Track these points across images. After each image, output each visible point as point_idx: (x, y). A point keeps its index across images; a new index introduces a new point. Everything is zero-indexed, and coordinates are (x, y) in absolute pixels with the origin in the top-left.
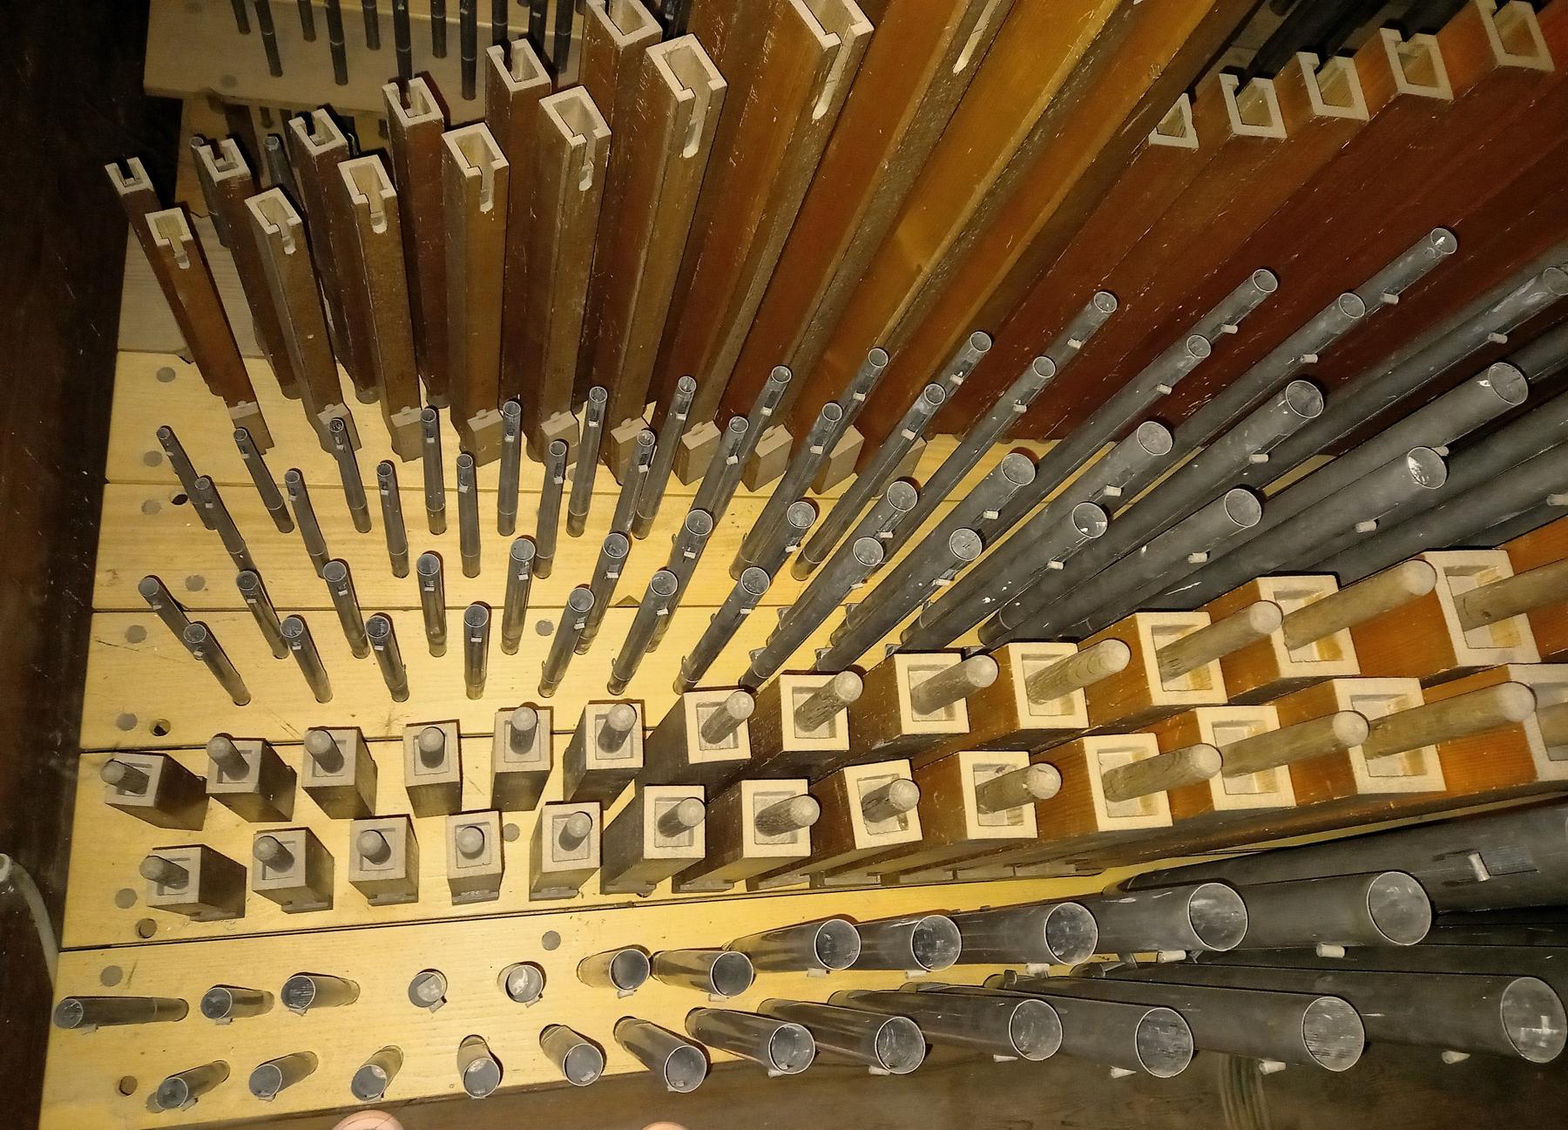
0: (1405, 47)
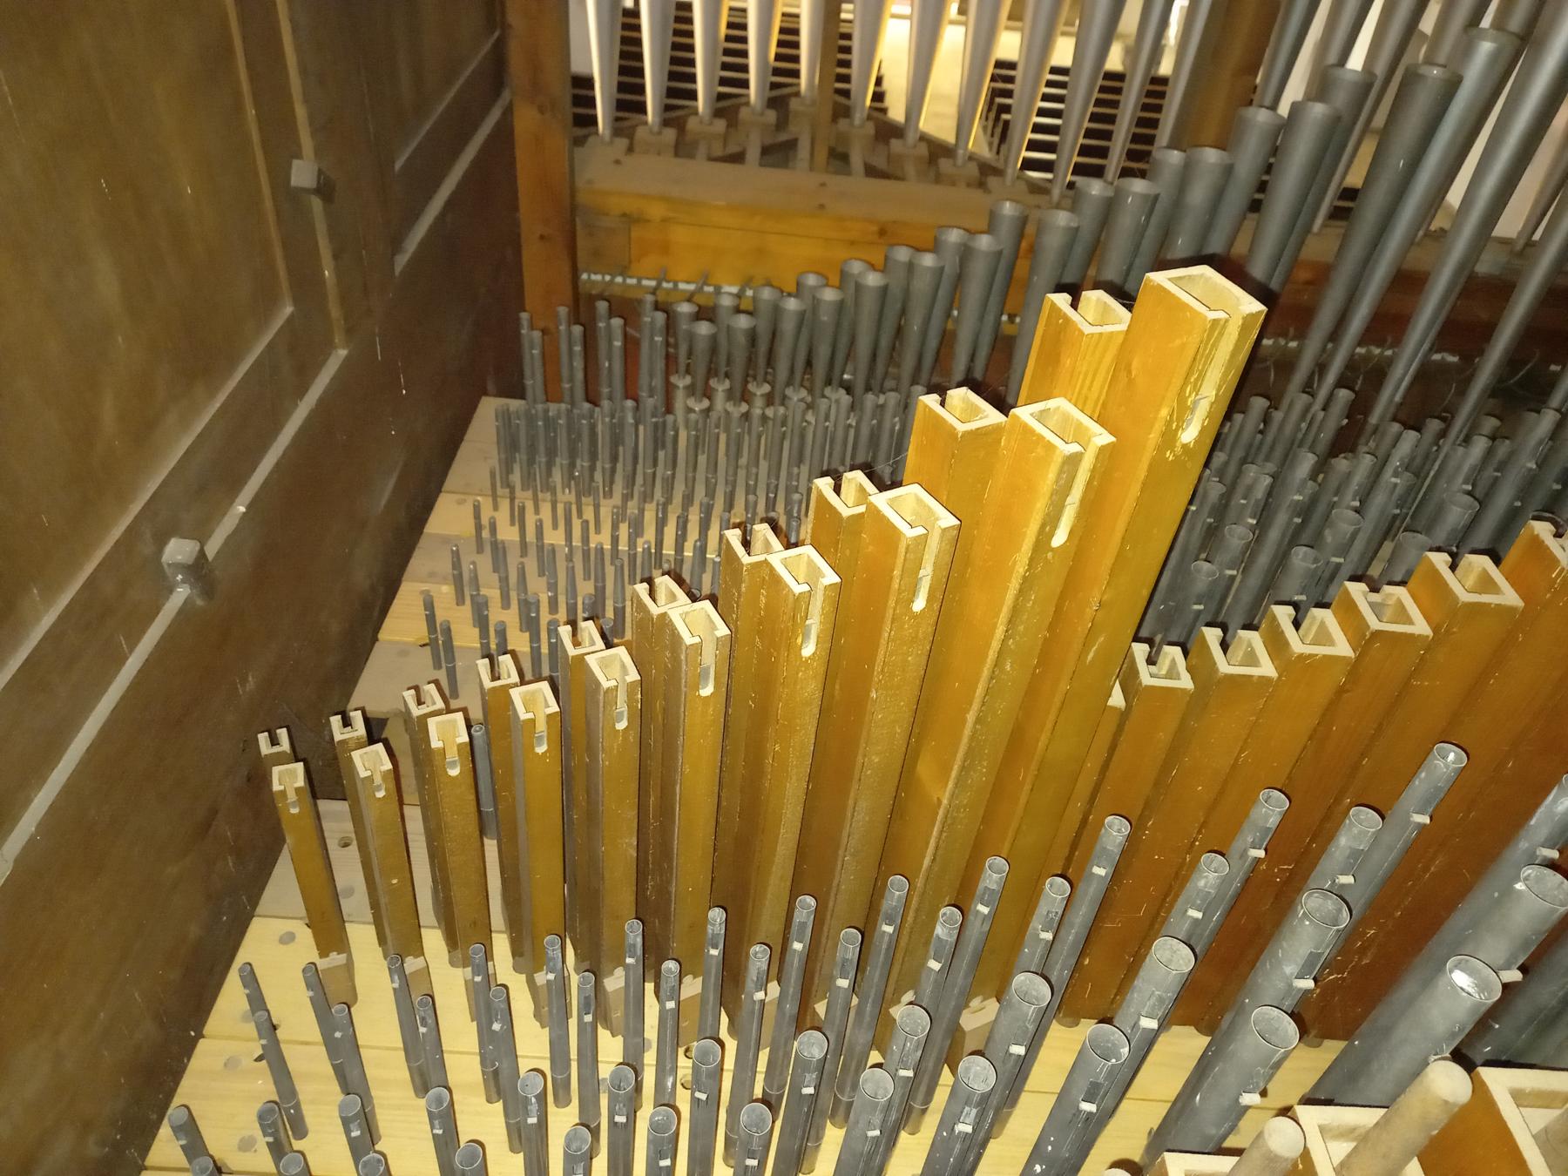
0: (1375, 597)
